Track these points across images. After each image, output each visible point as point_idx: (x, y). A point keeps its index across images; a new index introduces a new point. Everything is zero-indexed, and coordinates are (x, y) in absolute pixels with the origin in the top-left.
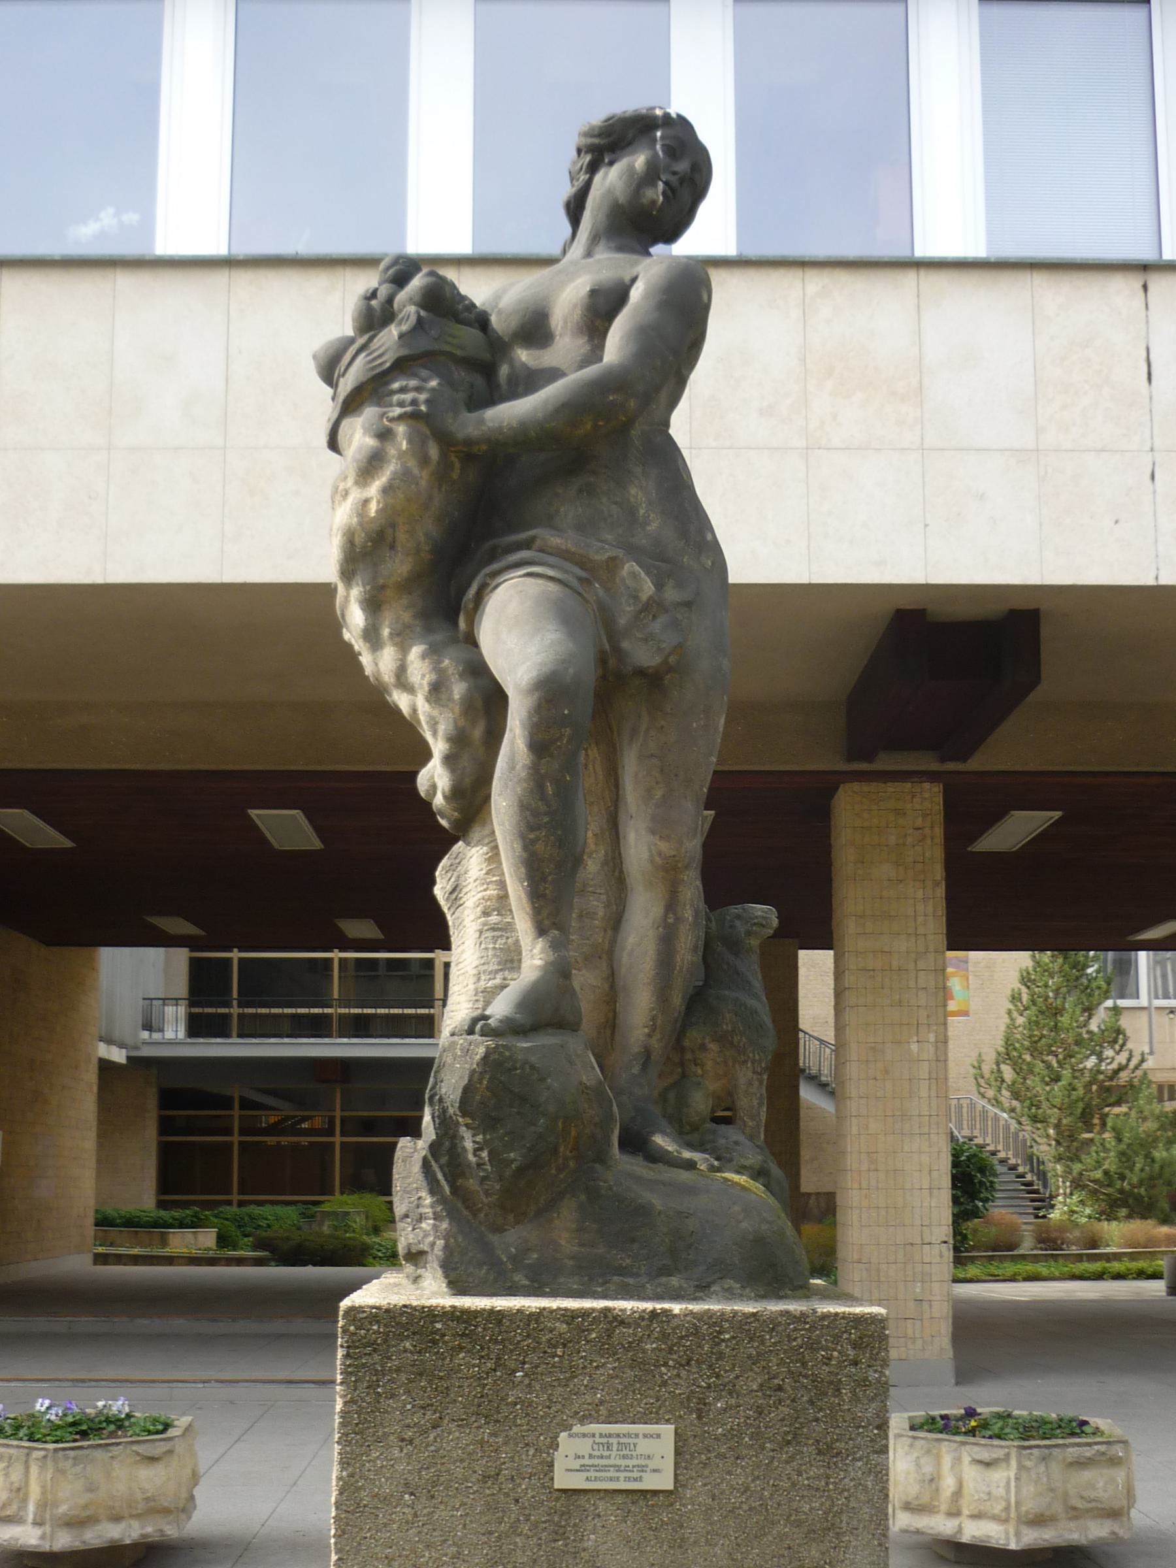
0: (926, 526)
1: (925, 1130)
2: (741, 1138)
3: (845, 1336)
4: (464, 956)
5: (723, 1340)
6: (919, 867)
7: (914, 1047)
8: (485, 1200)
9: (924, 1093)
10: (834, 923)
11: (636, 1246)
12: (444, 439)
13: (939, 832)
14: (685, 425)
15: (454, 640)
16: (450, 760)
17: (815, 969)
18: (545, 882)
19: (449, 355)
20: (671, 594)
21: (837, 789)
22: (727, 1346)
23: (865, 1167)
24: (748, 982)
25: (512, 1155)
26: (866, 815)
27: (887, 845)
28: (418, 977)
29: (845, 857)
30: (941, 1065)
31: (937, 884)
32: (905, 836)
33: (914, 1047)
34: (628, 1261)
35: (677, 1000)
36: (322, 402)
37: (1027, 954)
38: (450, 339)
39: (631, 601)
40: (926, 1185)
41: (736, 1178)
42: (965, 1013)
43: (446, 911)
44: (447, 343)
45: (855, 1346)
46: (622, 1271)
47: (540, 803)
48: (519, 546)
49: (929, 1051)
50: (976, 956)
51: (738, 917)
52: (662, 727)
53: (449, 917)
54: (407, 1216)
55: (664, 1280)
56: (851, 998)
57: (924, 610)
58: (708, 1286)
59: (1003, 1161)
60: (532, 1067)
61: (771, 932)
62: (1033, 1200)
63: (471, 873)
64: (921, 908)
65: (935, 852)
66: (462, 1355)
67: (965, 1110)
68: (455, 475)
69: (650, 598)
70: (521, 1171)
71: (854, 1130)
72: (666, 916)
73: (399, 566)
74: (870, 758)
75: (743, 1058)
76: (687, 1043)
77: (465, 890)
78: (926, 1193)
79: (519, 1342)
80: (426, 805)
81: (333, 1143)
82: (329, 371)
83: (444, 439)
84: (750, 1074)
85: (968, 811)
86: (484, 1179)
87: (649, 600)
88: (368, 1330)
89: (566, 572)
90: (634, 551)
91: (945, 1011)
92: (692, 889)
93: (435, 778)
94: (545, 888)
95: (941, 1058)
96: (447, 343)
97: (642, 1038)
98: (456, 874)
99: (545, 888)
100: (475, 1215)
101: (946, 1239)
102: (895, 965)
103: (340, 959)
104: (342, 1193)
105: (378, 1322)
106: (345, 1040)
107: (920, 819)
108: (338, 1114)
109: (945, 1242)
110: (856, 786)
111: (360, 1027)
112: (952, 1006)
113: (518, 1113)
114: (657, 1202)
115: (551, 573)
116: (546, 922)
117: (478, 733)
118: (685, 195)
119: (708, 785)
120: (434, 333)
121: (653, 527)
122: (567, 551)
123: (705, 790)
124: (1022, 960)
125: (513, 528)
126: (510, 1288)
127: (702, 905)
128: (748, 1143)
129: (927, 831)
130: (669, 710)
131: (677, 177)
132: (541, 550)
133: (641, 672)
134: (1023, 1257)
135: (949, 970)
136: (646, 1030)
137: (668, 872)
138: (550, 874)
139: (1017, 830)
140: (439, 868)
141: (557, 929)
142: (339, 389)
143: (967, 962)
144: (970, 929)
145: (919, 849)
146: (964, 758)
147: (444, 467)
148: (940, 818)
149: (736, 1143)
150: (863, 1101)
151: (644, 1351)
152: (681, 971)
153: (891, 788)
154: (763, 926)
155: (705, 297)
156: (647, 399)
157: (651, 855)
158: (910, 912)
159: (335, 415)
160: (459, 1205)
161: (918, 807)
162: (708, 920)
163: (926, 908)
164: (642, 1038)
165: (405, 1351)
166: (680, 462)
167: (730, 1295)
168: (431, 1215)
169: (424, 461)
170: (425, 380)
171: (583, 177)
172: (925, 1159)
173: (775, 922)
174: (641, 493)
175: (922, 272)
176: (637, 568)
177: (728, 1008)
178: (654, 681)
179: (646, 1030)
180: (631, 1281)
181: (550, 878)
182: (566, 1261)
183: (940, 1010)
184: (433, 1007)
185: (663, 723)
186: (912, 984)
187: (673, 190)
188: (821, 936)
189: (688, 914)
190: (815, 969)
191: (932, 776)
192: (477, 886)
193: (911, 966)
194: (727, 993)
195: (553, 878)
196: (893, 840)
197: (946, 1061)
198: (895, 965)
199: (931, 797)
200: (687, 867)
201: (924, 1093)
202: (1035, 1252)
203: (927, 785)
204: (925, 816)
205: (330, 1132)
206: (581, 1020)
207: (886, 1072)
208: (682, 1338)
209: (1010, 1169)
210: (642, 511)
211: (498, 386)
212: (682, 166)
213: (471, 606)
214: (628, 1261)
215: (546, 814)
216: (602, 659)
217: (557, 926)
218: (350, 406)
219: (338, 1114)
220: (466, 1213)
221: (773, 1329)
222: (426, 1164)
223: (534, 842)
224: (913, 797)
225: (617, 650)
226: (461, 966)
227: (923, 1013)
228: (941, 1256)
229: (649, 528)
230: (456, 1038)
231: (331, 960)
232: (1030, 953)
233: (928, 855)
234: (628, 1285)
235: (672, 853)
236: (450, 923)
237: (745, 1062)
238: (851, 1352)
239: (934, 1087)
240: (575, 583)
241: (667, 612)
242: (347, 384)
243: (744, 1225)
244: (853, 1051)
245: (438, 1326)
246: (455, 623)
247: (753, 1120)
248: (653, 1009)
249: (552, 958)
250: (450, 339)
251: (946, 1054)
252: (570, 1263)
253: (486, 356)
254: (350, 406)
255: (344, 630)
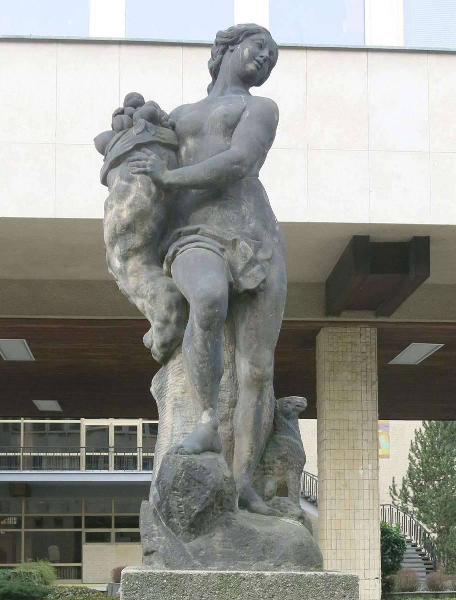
0: (370, 192)
1: (367, 517)
2: (291, 503)
3: (340, 585)
4: (166, 419)
5: (288, 587)
6: (364, 373)
7: (361, 472)
8: (182, 528)
9: (366, 497)
10: (317, 404)
11: (248, 547)
12: (158, 183)
13: (374, 354)
14: (266, 175)
15: (161, 275)
16: (160, 330)
17: (307, 428)
18: (207, 386)
19: (159, 143)
20: (261, 255)
21: (320, 330)
22: (289, 589)
23: (334, 537)
24: (294, 432)
25: (195, 507)
26: (335, 345)
27: (347, 361)
28: (69, 434)
29: (323, 367)
30: (376, 481)
31: (373, 383)
32: (357, 357)
33: (361, 472)
34: (245, 554)
35: (262, 441)
36: (98, 162)
37: (420, 422)
38: (160, 135)
39: (243, 259)
40: (367, 547)
41: (288, 520)
42: (388, 457)
43: (156, 399)
44: (159, 137)
45: (344, 589)
46: (242, 559)
47: (205, 351)
48: (196, 232)
49: (369, 475)
50: (393, 423)
51: (289, 402)
52: (256, 316)
53: (157, 402)
54: (146, 535)
55: (260, 563)
56: (327, 445)
57: (368, 236)
58: (280, 565)
59: (409, 542)
60: (204, 468)
61: (304, 409)
62: (425, 564)
63: (169, 381)
64: (364, 395)
65: (373, 366)
66: (175, 594)
67: (387, 512)
68: (162, 199)
69: (252, 258)
70: (199, 514)
71: (329, 517)
72: (257, 402)
73: (136, 240)
74: (338, 314)
75: (291, 467)
76: (266, 460)
77: (165, 390)
78: (367, 552)
79: (200, 588)
80: (148, 351)
81: (20, 533)
82: (102, 146)
83: (158, 183)
84: (294, 474)
85: (390, 343)
86: (182, 518)
87: (251, 258)
88: (134, 584)
89: (214, 245)
90: (244, 235)
91: (378, 455)
92: (269, 389)
93: (153, 339)
94: (207, 389)
95: (376, 479)
96: (159, 137)
97: (246, 457)
98: (161, 382)
99: (207, 389)
100: (177, 535)
101: (378, 577)
102: (351, 427)
103: (25, 423)
104: (26, 561)
105: (138, 580)
106: (28, 472)
107: (365, 348)
108: (23, 515)
109: (377, 578)
110: (330, 329)
111: (36, 464)
112: (381, 452)
113: (198, 488)
114: (258, 529)
115: (208, 246)
116: (207, 404)
117: (173, 317)
118: (266, 66)
119: (276, 342)
120: (153, 132)
121: (252, 225)
122: (214, 236)
123: (275, 344)
124: (418, 424)
125: (187, 223)
126: (193, 566)
127: (273, 397)
128: (294, 505)
129: (368, 354)
130: (260, 309)
131: (263, 58)
132: (202, 235)
133: (247, 291)
134: (420, 594)
135: (379, 431)
136: (248, 453)
137: (258, 383)
138: (209, 383)
139: (415, 354)
140: (153, 380)
141: (211, 407)
142: (108, 157)
143: (388, 427)
144: (392, 407)
145: (364, 364)
146: (389, 315)
147: (159, 194)
148: (375, 346)
149: (289, 505)
150: (333, 501)
151: (254, 592)
152: (264, 427)
153: (349, 330)
154: (300, 406)
155: (276, 118)
156: (251, 166)
157: (251, 374)
158: (359, 398)
159: (107, 170)
160: (170, 530)
161: (363, 341)
162: (276, 403)
163: (368, 397)
164: (246, 457)
165: (150, 592)
166: (264, 193)
167: (289, 568)
168: (157, 534)
169: (149, 194)
170: (149, 155)
171: (219, 56)
172: (367, 533)
173: (306, 405)
174: (247, 207)
175: (308, 51)
176: (246, 244)
177: (275, 448)
178: (252, 295)
179: (248, 453)
180: (246, 563)
181: (209, 385)
182: (218, 554)
183: (375, 452)
184: (80, 452)
185: (256, 314)
186: (360, 438)
187: (261, 64)
188: (310, 412)
189: (268, 401)
190: (307, 428)
191: (371, 324)
192: (174, 386)
193: (360, 428)
194: (284, 436)
195: (209, 383)
196: (350, 359)
197: (378, 479)
198: (351, 427)
199: (370, 336)
200: (267, 380)
201: (366, 497)
202: (426, 592)
203: (368, 329)
204: (367, 346)
205: (18, 525)
206: (221, 449)
207: (346, 486)
208: (270, 586)
209: (412, 546)
210: (247, 217)
211: (181, 156)
212: (265, 53)
213: (170, 259)
214: (245, 554)
215: (208, 356)
216: (231, 285)
217: (212, 406)
218: (114, 164)
219: (23, 515)
220: (173, 534)
221: (309, 582)
222: (155, 512)
223: (202, 369)
224: (361, 335)
225: (237, 281)
226: (164, 424)
227: (366, 453)
228: (375, 586)
229: (250, 225)
230: (169, 455)
231: (20, 424)
232: (422, 421)
233: (369, 367)
234: (245, 565)
235: (261, 373)
236: (158, 404)
237: (292, 468)
238: (343, 592)
239: (371, 494)
240: (218, 250)
241: (259, 264)
242: (112, 155)
243: (295, 538)
244: (328, 474)
245: (165, 581)
246: (162, 267)
247: (296, 495)
248: (252, 444)
249: (209, 421)
250: (160, 135)
251: (378, 477)
252: (220, 555)
253: (176, 143)
254: (114, 164)
255: (109, 268)
